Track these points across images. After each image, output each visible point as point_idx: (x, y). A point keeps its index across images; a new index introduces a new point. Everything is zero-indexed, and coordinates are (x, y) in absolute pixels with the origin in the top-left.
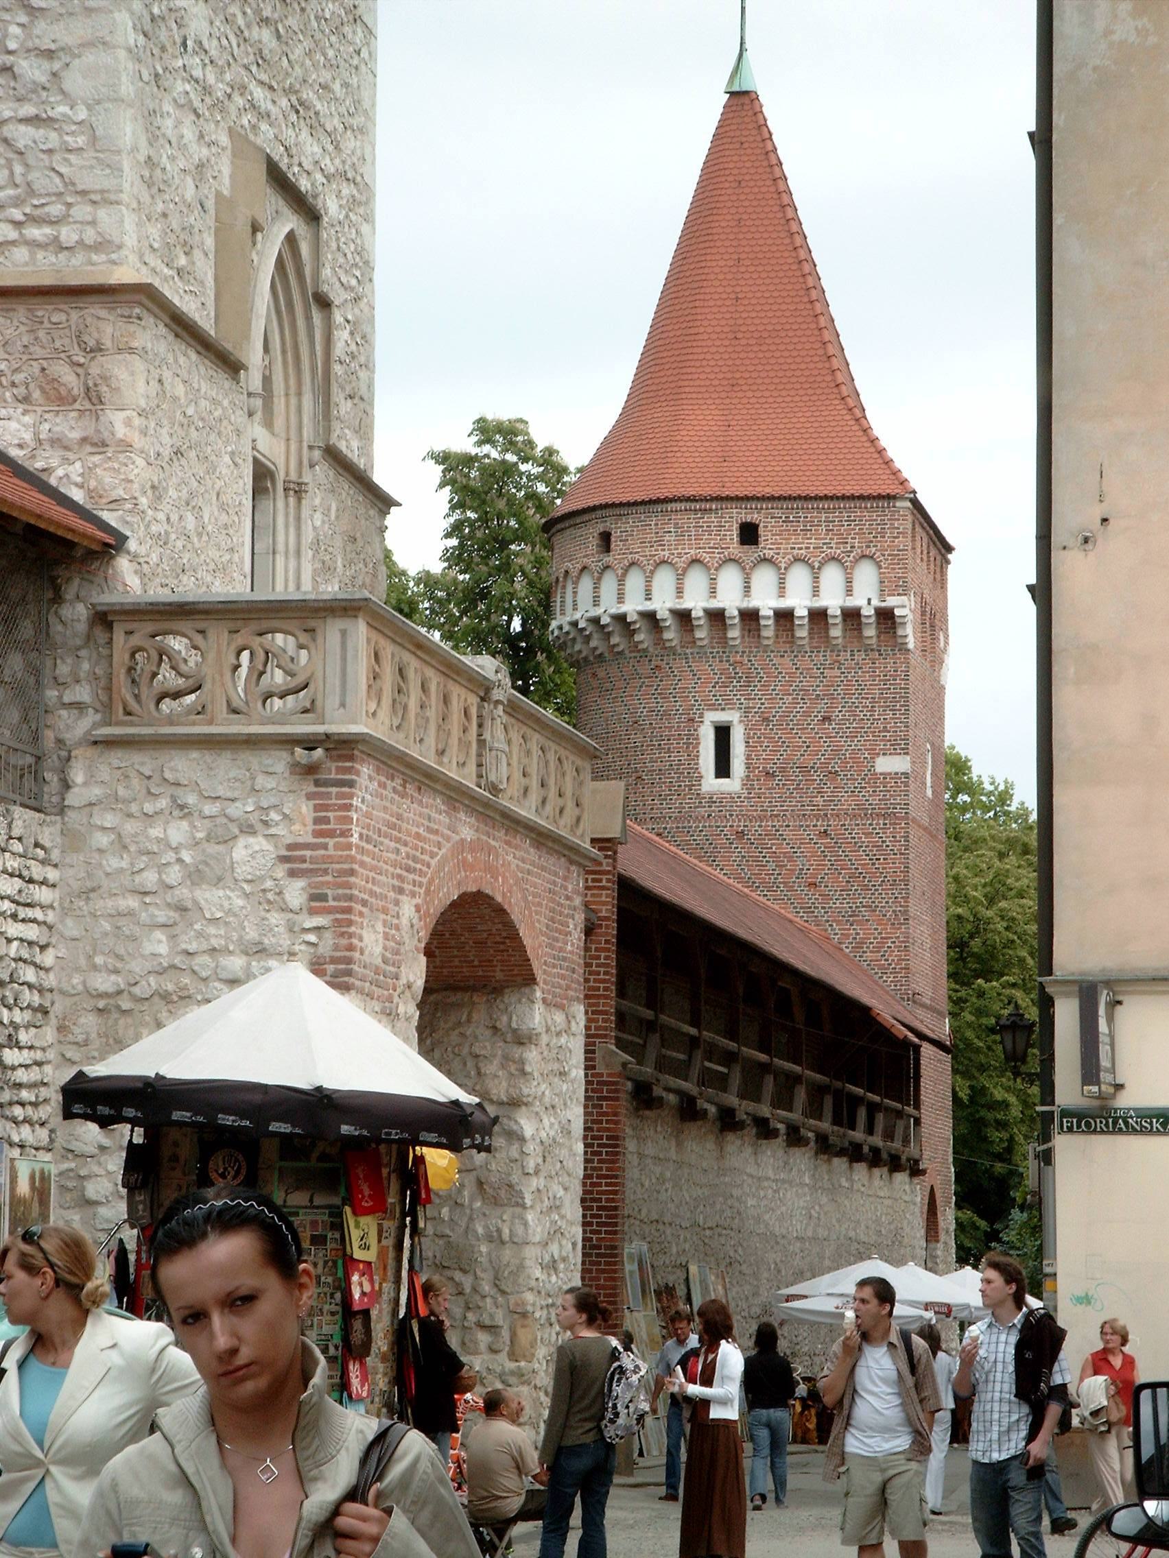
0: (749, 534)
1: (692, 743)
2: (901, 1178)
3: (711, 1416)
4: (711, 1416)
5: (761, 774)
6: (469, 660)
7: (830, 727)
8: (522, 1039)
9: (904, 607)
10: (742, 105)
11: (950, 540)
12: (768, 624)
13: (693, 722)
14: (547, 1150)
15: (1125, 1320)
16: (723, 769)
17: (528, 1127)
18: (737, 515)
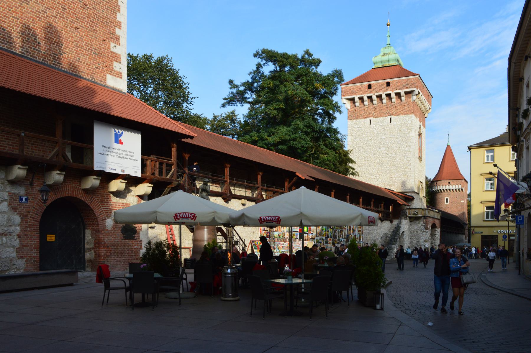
0: (449, 183)
5: (451, 202)
9: (464, 189)
10: (448, 147)
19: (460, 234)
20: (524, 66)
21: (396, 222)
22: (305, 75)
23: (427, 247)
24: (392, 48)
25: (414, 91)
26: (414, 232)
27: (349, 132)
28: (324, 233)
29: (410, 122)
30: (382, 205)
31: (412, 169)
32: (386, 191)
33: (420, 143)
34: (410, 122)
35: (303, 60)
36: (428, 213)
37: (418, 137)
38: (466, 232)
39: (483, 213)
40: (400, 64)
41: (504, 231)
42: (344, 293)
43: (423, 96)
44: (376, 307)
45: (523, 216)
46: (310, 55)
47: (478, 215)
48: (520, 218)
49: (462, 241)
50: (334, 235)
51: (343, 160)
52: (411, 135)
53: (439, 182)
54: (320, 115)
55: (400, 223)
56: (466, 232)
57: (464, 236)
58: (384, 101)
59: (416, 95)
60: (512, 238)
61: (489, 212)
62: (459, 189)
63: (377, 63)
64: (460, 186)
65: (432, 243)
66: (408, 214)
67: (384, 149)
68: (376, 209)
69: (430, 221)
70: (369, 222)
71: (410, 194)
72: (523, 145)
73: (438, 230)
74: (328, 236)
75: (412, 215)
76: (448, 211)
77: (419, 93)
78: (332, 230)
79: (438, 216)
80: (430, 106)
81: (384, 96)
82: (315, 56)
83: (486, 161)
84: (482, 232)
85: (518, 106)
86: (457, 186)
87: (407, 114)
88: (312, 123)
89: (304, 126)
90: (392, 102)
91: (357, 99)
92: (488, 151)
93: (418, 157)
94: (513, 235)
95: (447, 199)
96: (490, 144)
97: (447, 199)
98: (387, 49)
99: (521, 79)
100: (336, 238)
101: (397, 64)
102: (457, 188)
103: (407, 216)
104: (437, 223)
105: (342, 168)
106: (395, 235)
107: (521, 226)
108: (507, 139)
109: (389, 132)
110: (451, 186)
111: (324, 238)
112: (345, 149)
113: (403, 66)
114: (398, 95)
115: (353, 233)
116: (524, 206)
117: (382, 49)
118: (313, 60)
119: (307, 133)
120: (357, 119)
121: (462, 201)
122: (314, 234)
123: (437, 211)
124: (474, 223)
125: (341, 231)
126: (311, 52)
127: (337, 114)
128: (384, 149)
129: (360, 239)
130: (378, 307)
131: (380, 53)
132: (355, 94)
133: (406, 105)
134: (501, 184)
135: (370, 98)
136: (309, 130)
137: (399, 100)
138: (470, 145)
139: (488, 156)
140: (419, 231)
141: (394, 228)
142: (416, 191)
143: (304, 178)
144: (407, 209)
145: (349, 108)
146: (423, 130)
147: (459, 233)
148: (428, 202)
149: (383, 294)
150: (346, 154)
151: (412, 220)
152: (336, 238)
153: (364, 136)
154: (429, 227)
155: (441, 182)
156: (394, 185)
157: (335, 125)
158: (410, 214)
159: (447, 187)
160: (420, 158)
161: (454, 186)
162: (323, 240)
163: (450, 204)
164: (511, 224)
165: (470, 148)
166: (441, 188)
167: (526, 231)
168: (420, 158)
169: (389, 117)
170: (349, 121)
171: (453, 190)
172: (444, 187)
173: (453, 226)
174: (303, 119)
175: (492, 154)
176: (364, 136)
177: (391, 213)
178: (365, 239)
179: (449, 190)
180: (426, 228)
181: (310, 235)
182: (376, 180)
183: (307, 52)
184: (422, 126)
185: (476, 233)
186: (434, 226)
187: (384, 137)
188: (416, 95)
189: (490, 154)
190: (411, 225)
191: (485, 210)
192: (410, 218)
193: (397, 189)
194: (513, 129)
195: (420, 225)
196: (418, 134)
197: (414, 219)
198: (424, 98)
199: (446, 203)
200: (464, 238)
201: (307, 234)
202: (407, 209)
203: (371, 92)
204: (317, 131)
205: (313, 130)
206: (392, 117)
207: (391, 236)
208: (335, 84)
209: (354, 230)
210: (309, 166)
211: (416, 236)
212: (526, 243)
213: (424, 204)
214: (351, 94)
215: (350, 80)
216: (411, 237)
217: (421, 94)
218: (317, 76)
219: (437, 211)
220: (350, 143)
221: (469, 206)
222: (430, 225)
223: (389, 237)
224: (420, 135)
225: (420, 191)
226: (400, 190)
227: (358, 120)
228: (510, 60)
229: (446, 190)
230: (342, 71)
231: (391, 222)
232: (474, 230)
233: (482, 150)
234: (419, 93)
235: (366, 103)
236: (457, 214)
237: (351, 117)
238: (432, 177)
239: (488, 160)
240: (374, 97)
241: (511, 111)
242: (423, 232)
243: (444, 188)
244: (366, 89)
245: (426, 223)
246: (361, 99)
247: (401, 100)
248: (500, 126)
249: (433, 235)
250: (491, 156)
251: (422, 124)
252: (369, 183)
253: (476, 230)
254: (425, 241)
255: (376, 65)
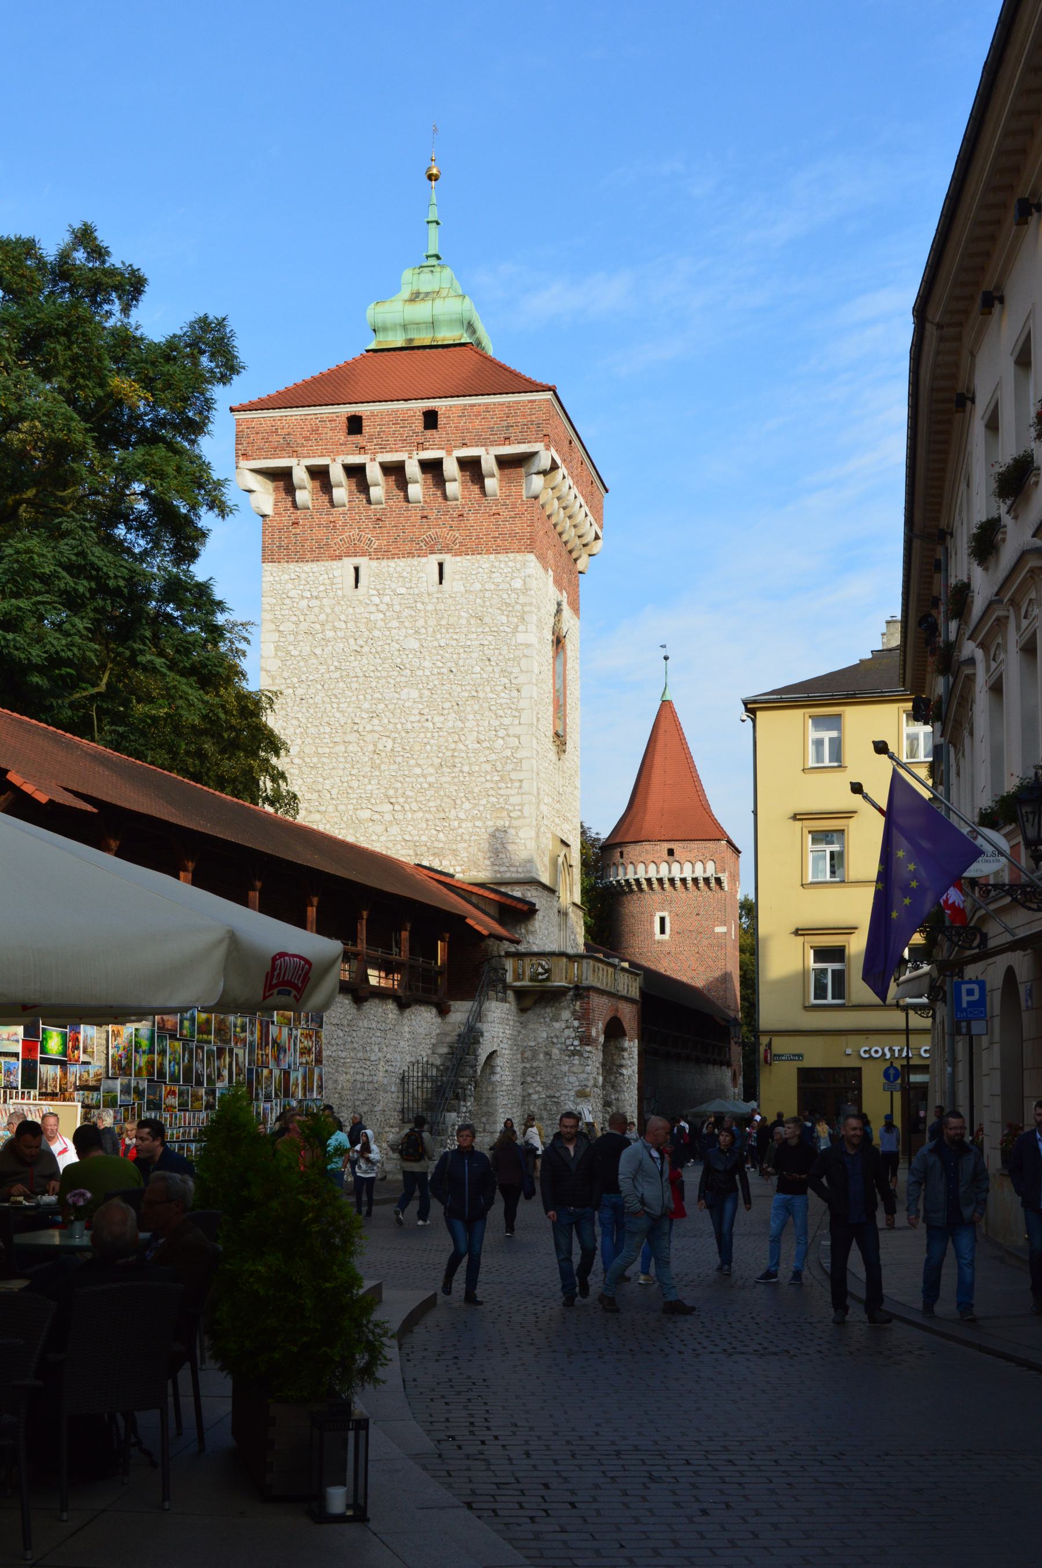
0: (671, 852)
1: (652, 923)
2: (724, 1068)
3: (77, 1160)
4: (77, 1160)
5: (676, 933)
6: (611, 960)
7: (699, 917)
8: (624, 1050)
9: (724, 877)
10: (666, 707)
11: (740, 849)
12: (678, 883)
13: (652, 916)
14: (629, 1077)
15: (783, 1111)
16: (663, 931)
17: (624, 1071)
18: (666, 846)
19: (715, 1063)
20: (978, 341)
21: (460, 1012)
22: (66, 333)
23: (589, 1118)
24: (447, 272)
25: (534, 454)
26: (535, 1056)
27: (267, 616)
28: (142, 1060)
29: (518, 584)
30: (405, 935)
31: (526, 786)
32: (422, 875)
33: (560, 677)
34: (518, 584)
35: (63, 270)
36: (594, 975)
37: (549, 649)
38: (736, 1053)
39: (805, 973)
40: (479, 343)
41: (890, 1049)
42: (147, 1420)
43: (569, 481)
44: (322, 1499)
45: (982, 984)
46: (98, 252)
47: (784, 982)
48: (970, 992)
49: (720, 1092)
50: (188, 1070)
51: (240, 737)
52: (521, 638)
53: (631, 851)
54: (141, 525)
55: (479, 1016)
56: (736, 1053)
57: (728, 1073)
58: (415, 490)
59: (544, 473)
60: (914, 1078)
61: (824, 971)
62: (707, 880)
63: (385, 329)
64: (711, 867)
65: (607, 1104)
66: (509, 978)
67: (415, 694)
68: (379, 953)
69: (601, 1008)
70: (269, 986)
71: (517, 893)
72: (971, 679)
73: (632, 1047)
74: (161, 1074)
75: (526, 983)
76: (667, 967)
77: (554, 467)
78: (178, 1045)
79: (631, 987)
80: (596, 527)
81: (413, 469)
82: (121, 255)
83: (811, 763)
84: (800, 1056)
85: (943, 525)
86: (699, 866)
87: (507, 551)
88: (98, 555)
89: (60, 564)
90: (445, 497)
91: (300, 475)
92: (819, 722)
93: (550, 733)
94: (923, 1069)
95: (662, 920)
96: (826, 694)
97: (662, 920)
98: (426, 276)
99: (964, 400)
100: (199, 1083)
101: (465, 339)
102: (699, 873)
103: (506, 987)
104: (628, 1015)
105: (229, 766)
106: (460, 1069)
107: (977, 1027)
108: (895, 673)
109: (432, 622)
110: (676, 867)
111: (144, 1085)
112: (250, 686)
113: (491, 351)
114: (471, 467)
115: (277, 1059)
116: (984, 938)
117: (407, 275)
118: (112, 272)
119: (72, 602)
120: (302, 559)
121: (720, 929)
122: (97, 1065)
123: (626, 965)
124: (769, 1015)
125: (221, 1052)
126: (103, 237)
127: (207, 519)
128: (415, 694)
129: (307, 1088)
130: (337, 1499)
131: (397, 289)
132: (295, 454)
133: (505, 514)
134: (895, 832)
135: (356, 472)
136: (83, 586)
137: (476, 489)
138: (751, 693)
139: (819, 743)
140: (555, 1051)
141: (452, 1038)
142: (545, 879)
143: (42, 798)
144: (508, 955)
145: (269, 510)
146: (570, 622)
147: (708, 1062)
148: (588, 929)
149: (363, 1425)
150: (250, 708)
151: (528, 1003)
152: (199, 1083)
153: (330, 634)
154: (597, 1031)
155: (638, 848)
156: (455, 853)
157: (200, 570)
158: (518, 977)
159: (664, 872)
160: (560, 739)
161: (688, 866)
162: (139, 1093)
163: (678, 941)
164: (918, 1021)
165: (752, 707)
166: (641, 874)
167: (996, 1048)
168: (560, 739)
169: (433, 560)
170: (268, 567)
171: (683, 881)
172: (652, 868)
173: (687, 1028)
174: (58, 534)
175: (834, 734)
176: (330, 634)
177: (441, 973)
178: (329, 1085)
179: (672, 881)
180: (586, 1040)
181: (75, 1071)
182: (379, 829)
183: (85, 236)
184: (565, 606)
185: (779, 1057)
186: (614, 1030)
187: (414, 644)
188: (544, 473)
189: (827, 735)
190: (524, 1025)
191: (812, 964)
192: (521, 994)
193: (468, 865)
194: (920, 623)
195: (560, 1025)
196: (550, 637)
197: (536, 999)
198: (575, 491)
199: (658, 936)
200: (726, 1079)
201: (63, 1064)
202: (508, 955)
203: (362, 449)
204: (117, 592)
205: (102, 588)
206: (447, 559)
207: (444, 1070)
208: (199, 381)
209: (280, 1049)
210: (78, 747)
211: (544, 1074)
212: (997, 1102)
213: (575, 935)
214: (275, 453)
215: (272, 392)
216: (526, 1077)
217: (562, 470)
218: (125, 341)
219: (626, 965)
220: (273, 665)
221: (750, 949)
222: (601, 1025)
223: (433, 1080)
224: (559, 642)
225: (561, 879)
226: (482, 873)
227: (308, 567)
228: (921, 311)
229: (660, 881)
230: (232, 325)
231: (443, 1011)
232: (769, 1045)
233: (796, 717)
234: (554, 467)
235: (340, 494)
236: (699, 982)
237: (281, 545)
238: (603, 830)
239: (819, 757)
240: (374, 472)
241: (916, 543)
242: (574, 1053)
243: (652, 873)
244: (342, 436)
245: (584, 1017)
246: (320, 475)
247: (484, 493)
248: (864, 612)
249: (611, 1068)
250: (831, 740)
251: (564, 598)
252: (350, 839)
253: (780, 1045)
254: (582, 1094)
255: (381, 337)
